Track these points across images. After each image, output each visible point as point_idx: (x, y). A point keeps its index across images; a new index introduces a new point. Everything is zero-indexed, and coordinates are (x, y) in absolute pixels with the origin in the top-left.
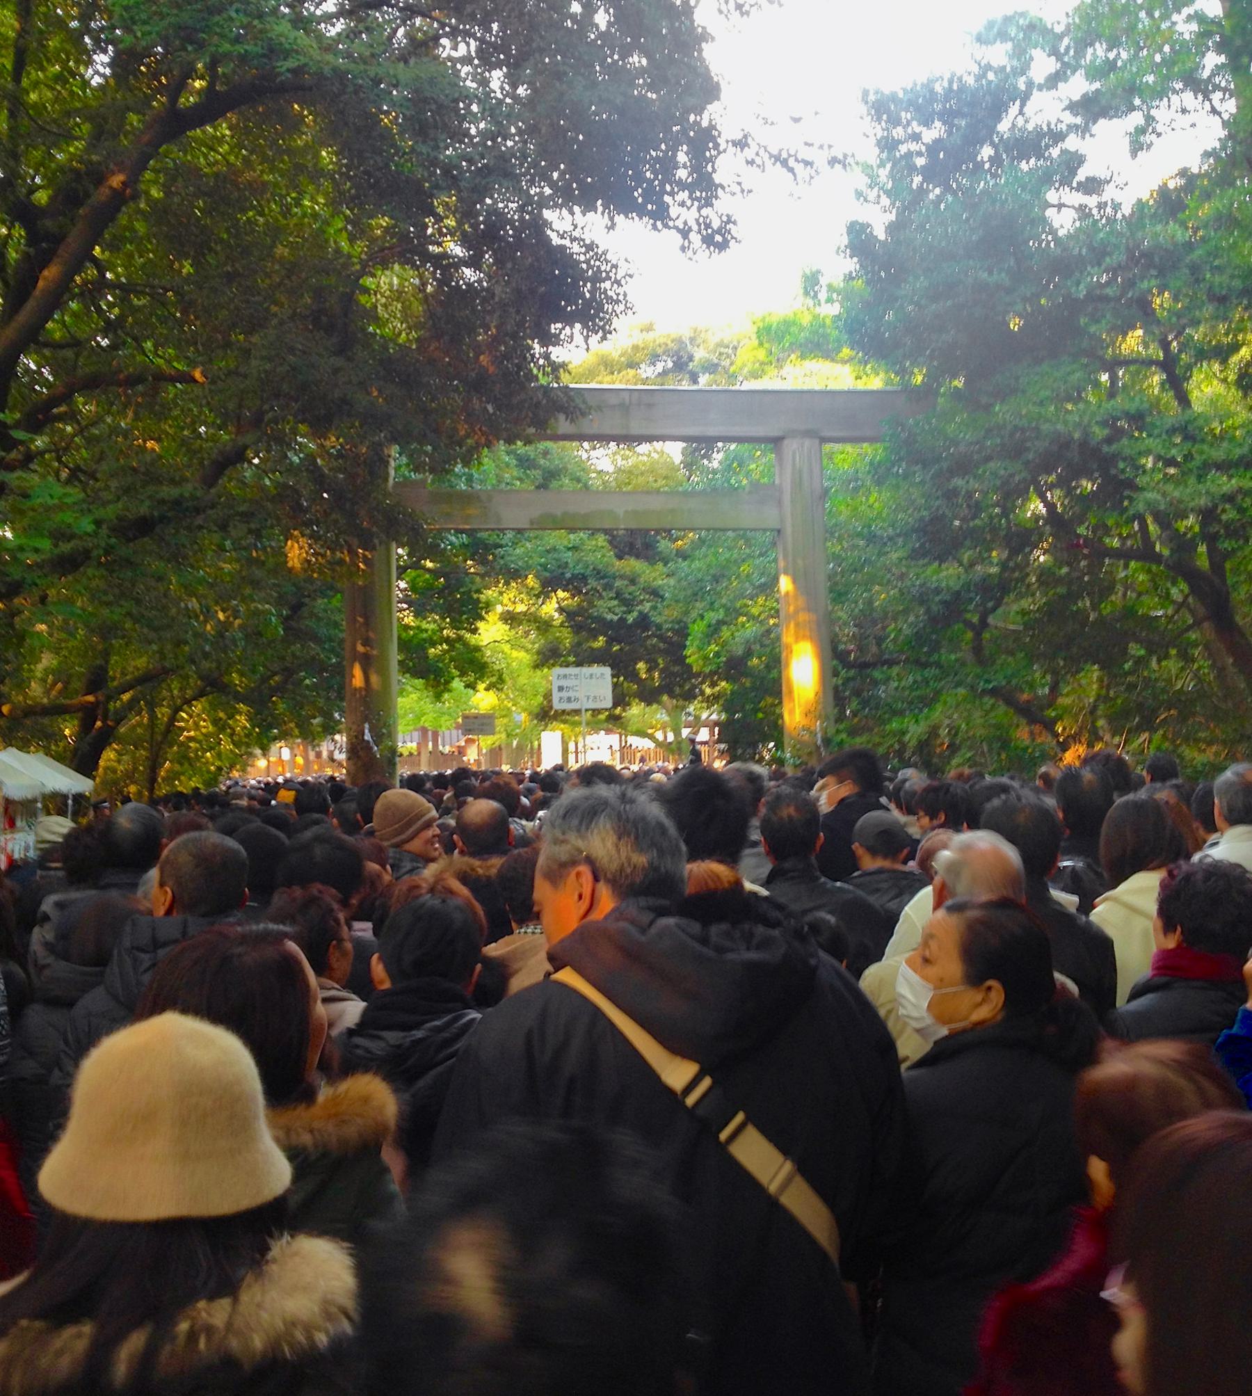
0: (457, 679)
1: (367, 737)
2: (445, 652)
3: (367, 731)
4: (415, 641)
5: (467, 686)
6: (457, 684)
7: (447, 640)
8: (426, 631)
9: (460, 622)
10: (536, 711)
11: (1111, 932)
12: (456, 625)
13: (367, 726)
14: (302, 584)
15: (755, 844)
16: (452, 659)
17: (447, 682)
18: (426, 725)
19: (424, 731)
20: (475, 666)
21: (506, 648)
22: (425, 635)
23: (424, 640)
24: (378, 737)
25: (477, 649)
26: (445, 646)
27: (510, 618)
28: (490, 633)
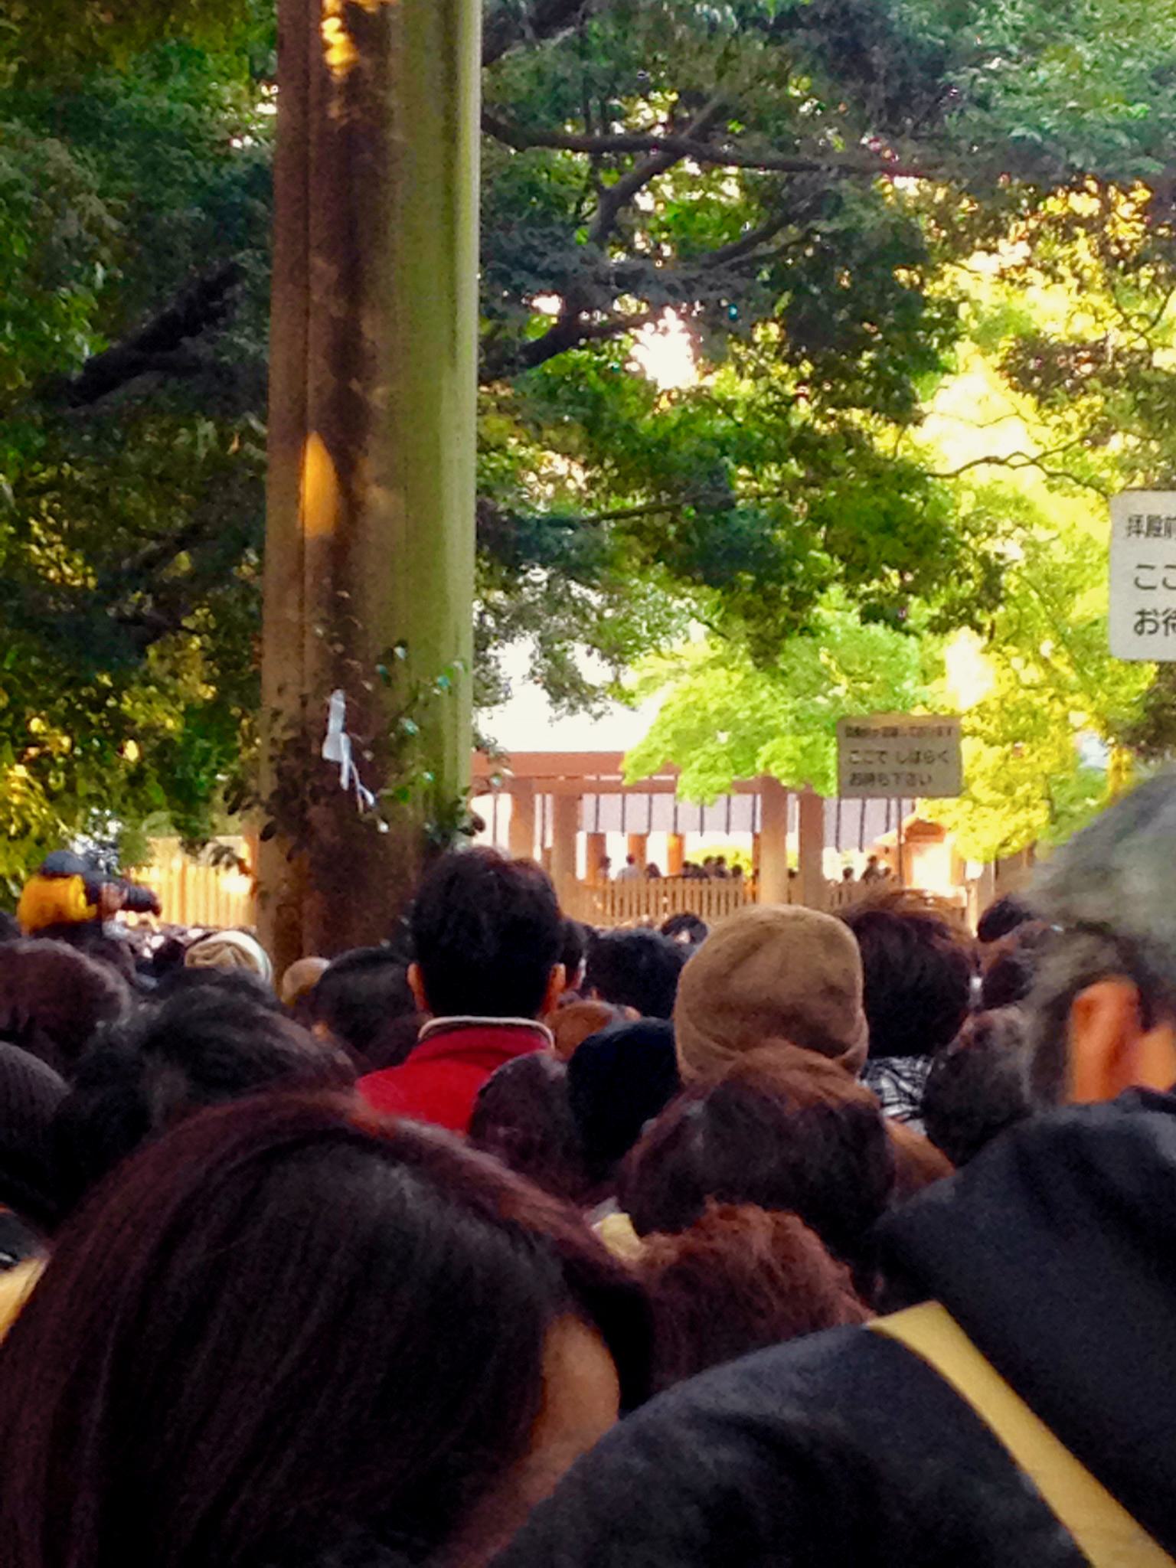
0: (836, 591)
1: (337, 748)
2: (792, 487)
3: (335, 724)
4: (687, 446)
5: (870, 615)
6: (834, 610)
7: (803, 444)
8: (729, 408)
9: (850, 376)
10: (1131, 715)
11: (154, 889)
12: (832, 378)
13: (337, 702)
14: (237, 196)
15: (119, 609)
16: (819, 516)
17: (802, 601)
18: (775, 772)
19: (771, 792)
20: (904, 544)
21: (1029, 482)
22: (721, 425)
23: (722, 444)
24: (380, 753)
25: (910, 477)
26: (793, 466)
27: (1040, 370)
28: (965, 427)
